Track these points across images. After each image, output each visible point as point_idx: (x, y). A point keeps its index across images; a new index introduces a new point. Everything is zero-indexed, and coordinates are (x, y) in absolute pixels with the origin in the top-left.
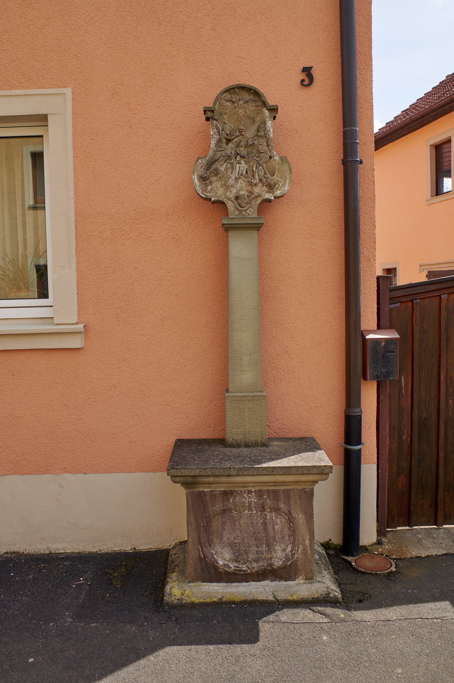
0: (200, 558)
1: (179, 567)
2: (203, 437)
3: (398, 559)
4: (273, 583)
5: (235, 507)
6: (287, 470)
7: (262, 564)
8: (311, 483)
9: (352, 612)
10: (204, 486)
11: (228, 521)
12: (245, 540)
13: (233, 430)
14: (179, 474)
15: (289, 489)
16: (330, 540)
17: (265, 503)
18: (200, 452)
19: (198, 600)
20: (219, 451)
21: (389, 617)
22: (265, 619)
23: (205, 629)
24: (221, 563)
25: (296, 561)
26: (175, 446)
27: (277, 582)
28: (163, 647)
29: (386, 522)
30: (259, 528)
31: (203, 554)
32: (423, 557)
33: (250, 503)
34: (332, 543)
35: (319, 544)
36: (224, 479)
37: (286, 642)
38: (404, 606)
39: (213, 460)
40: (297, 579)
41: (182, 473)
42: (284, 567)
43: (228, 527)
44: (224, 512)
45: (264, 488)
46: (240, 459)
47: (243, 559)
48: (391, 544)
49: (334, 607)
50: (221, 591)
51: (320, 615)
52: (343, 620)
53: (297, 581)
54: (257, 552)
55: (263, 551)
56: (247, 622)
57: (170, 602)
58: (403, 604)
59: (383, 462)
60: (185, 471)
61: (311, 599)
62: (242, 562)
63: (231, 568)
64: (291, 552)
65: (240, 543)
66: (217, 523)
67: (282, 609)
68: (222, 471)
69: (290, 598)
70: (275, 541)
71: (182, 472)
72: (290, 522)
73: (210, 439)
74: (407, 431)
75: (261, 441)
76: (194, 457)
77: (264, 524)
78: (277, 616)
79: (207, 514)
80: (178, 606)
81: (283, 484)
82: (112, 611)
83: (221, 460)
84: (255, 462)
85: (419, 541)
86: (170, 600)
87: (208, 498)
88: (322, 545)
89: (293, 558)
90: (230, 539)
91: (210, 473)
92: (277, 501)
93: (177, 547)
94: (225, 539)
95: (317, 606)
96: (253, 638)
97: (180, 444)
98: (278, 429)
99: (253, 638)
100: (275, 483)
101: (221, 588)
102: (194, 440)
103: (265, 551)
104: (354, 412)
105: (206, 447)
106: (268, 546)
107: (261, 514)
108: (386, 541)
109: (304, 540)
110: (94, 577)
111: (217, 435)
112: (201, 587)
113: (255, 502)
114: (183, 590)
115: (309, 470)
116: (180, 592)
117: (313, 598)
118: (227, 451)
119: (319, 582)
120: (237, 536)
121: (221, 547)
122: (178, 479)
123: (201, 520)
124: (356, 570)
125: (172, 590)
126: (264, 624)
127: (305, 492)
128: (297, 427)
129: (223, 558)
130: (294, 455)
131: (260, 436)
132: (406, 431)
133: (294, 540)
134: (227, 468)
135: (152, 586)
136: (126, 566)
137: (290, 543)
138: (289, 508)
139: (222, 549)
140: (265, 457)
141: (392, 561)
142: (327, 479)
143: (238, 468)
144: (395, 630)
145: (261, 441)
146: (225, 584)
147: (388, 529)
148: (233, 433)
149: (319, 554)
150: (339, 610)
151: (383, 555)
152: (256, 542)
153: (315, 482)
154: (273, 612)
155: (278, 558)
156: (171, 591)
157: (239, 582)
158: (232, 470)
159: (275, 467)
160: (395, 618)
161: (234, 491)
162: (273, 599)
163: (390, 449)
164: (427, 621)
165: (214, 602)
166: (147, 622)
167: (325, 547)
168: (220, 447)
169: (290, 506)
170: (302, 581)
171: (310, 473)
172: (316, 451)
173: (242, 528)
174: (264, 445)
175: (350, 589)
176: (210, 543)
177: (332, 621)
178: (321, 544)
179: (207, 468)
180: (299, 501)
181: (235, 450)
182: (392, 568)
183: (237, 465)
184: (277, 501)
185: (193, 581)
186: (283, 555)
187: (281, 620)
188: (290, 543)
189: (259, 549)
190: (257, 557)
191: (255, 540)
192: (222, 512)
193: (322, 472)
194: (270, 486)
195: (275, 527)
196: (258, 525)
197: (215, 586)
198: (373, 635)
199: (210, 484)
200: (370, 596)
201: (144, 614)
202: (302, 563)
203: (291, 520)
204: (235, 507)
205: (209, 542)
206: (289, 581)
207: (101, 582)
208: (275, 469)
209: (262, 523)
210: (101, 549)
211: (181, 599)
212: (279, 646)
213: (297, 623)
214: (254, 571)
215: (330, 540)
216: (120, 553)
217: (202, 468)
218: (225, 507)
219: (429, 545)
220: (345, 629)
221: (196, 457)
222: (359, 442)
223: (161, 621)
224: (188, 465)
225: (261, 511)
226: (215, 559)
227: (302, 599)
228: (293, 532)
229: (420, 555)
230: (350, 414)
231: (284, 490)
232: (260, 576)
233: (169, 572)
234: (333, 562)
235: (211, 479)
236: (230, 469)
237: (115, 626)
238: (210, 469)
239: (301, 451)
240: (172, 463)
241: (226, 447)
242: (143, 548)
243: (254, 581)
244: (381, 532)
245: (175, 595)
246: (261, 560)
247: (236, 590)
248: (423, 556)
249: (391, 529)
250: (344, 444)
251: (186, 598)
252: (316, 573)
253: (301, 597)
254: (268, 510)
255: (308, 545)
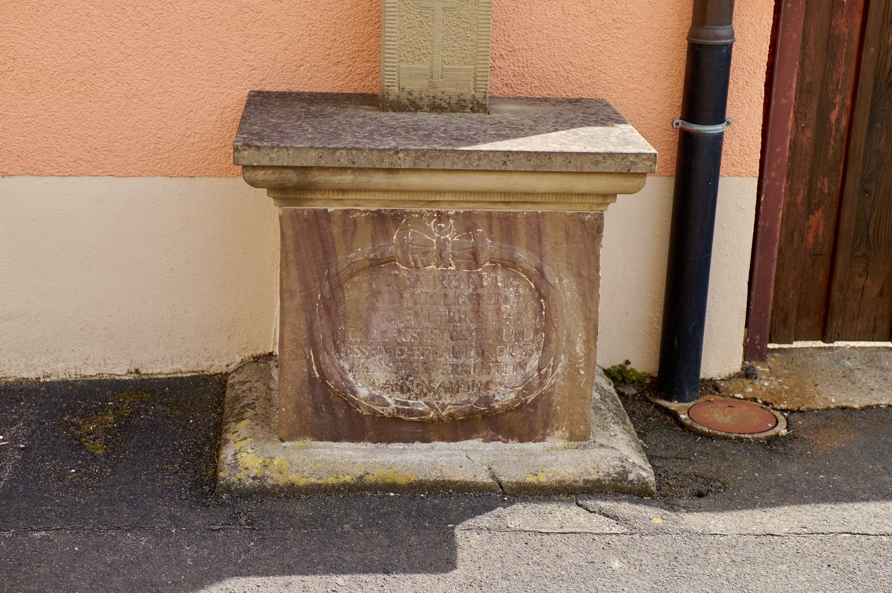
0: (311, 380)
1: (253, 409)
2: (319, 90)
3: (792, 412)
4: (491, 446)
5: (405, 253)
6: (541, 163)
7: (465, 398)
8: (599, 200)
9: (682, 515)
10: (326, 196)
11: (384, 288)
12: (426, 336)
13: (403, 65)
14: (265, 162)
15: (543, 213)
16: (628, 362)
17: (481, 245)
18: (317, 117)
19: (304, 479)
20: (363, 117)
21: (770, 528)
22: (470, 522)
23: (324, 543)
24: (363, 392)
25: (550, 394)
26: (248, 103)
27: (500, 443)
28: (220, 578)
29: (768, 326)
30: (463, 308)
31: (320, 370)
32: (855, 409)
33: (442, 245)
34: (632, 370)
35: (602, 372)
36: (380, 180)
37: (522, 570)
38: (807, 507)
39: (352, 134)
40: (548, 438)
41: (271, 159)
42: (520, 408)
43: (383, 304)
44: (375, 264)
45: (479, 209)
46: (420, 133)
47: (418, 385)
48: (777, 377)
49: (637, 503)
50: (363, 460)
51: (603, 518)
52: (659, 531)
53: (549, 443)
54: (455, 367)
55: (469, 366)
56: (425, 528)
57: (234, 483)
58: (805, 502)
59: (773, 175)
60: (281, 153)
61: (581, 484)
62: (417, 391)
63: (388, 405)
64: (539, 370)
65: (412, 344)
66: (356, 293)
67: (512, 504)
68: (375, 156)
69: (531, 479)
70: (501, 342)
71: (273, 155)
72: (541, 296)
73: (338, 94)
74: (841, 99)
75: (473, 96)
76: (300, 126)
77: (476, 298)
78: (499, 517)
79: (333, 270)
80: (255, 493)
81: (527, 199)
82: (86, 504)
83: (371, 133)
84: (462, 140)
85: (848, 374)
86: (233, 479)
87: (336, 230)
88: (607, 373)
89: (541, 384)
90: (389, 335)
91: (344, 162)
92: (511, 242)
93: (247, 368)
94: (375, 333)
95: (596, 498)
96: (442, 560)
97: (259, 101)
98: (515, 76)
99: (442, 560)
100: (508, 196)
101: (361, 454)
102: (298, 94)
103: (475, 365)
104: (716, 34)
105: (330, 109)
106: (482, 353)
107: (468, 274)
108: (764, 372)
109: (571, 342)
110: (33, 432)
111: (356, 85)
112: (312, 451)
113: (454, 243)
114: (267, 455)
115: (597, 163)
116: (260, 461)
117: (586, 482)
118: (387, 117)
119: (602, 446)
120: (406, 328)
121: (364, 354)
122: (260, 175)
123: (318, 284)
124: (690, 431)
125: (238, 456)
126: (468, 532)
127: (582, 222)
128: (563, 73)
129: (369, 380)
130: (556, 130)
131: (472, 84)
132: (838, 99)
133: (548, 340)
134: (389, 150)
135: (185, 452)
136: (115, 409)
137: (538, 349)
138: (539, 262)
139: (368, 358)
140: (485, 131)
141: (778, 414)
142: (639, 188)
143: (416, 151)
144: (785, 554)
145: (473, 96)
146: (370, 445)
147: (770, 346)
148: (402, 75)
149: (601, 390)
150: (648, 509)
151: (755, 400)
152: (453, 343)
153: (608, 197)
154: (489, 508)
155: (505, 387)
156: (236, 459)
157: (405, 442)
158: (401, 155)
159: (511, 152)
160: (786, 530)
161: (404, 212)
162: (490, 481)
163: (794, 144)
164: (863, 538)
165: (345, 484)
166: (177, 526)
167: (614, 379)
168: (367, 110)
169: (541, 257)
170: (561, 443)
171: (600, 170)
172: (612, 126)
173: (419, 307)
174: (479, 107)
175: (675, 470)
176: (338, 343)
177: (634, 531)
178: (605, 371)
179: (337, 149)
180: (565, 245)
181: (405, 117)
182: (777, 429)
183: (415, 145)
184: (511, 242)
185: (291, 437)
186: (519, 378)
187: (509, 525)
188: (538, 349)
189: (460, 361)
190: (454, 381)
191: (452, 338)
192: (371, 265)
193: (628, 169)
194: (495, 203)
195: (503, 308)
196: (461, 301)
197: (346, 449)
198: (734, 561)
199: (343, 191)
200: (723, 484)
201: (170, 511)
202: (564, 397)
203: (541, 292)
204: (405, 253)
205: (334, 341)
206: (529, 440)
207: (54, 442)
208: (511, 157)
209: (470, 297)
210: (48, 371)
211: (263, 478)
212: (506, 577)
213: (548, 533)
214: (444, 414)
215: (628, 362)
216: (99, 381)
217: (324, 148)
218: (378, 253)
219: (872, 383)
220: (665, 547)
221: (306, 127)
222: (719, 117)
223: (214, 524)
224: (286, 140)
225: (469, 267)
226: (348, 381)
227: (559, 482)
228: (546, 320)
229: (849, 404)
230: (702, 41)
231: (529, 217)
232: (458, 427)
233: (230, 419)
234: (634, 412)
235: (347, 179)
236: (398, 152)
237: (96, 536)
238: (344, 152)
239: (574, 124)
240: (245, 136)
241: (383, 109)
242: (158, 371)
243: (442, 439)
244: (753, 350)
245: (246, 469)
246: (463, 388)
247: (399, 458)
248: (856, 406)
249: (777, 346)
250: (680, 121)
251: (276, 475)
252: (594, 428)
253: (558, 478)
254: (487, 264)
255: (581, 354)
